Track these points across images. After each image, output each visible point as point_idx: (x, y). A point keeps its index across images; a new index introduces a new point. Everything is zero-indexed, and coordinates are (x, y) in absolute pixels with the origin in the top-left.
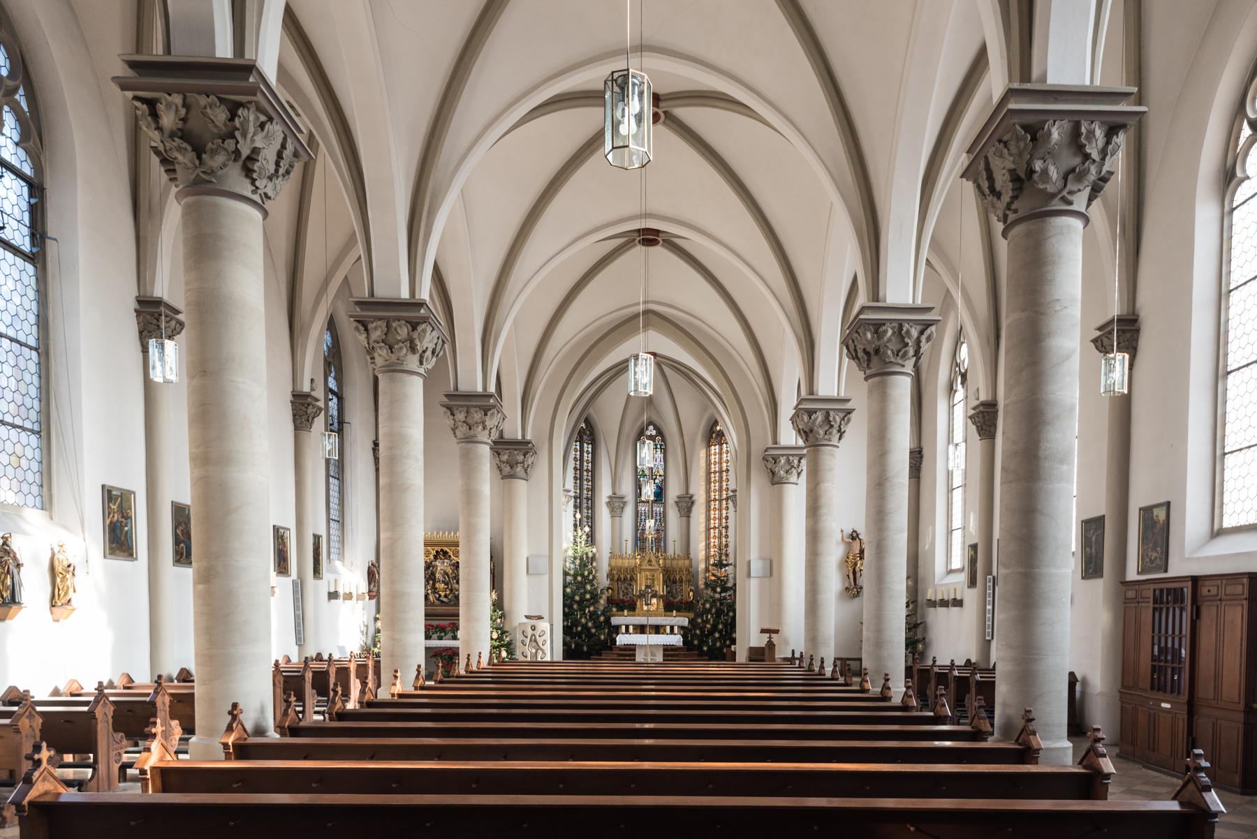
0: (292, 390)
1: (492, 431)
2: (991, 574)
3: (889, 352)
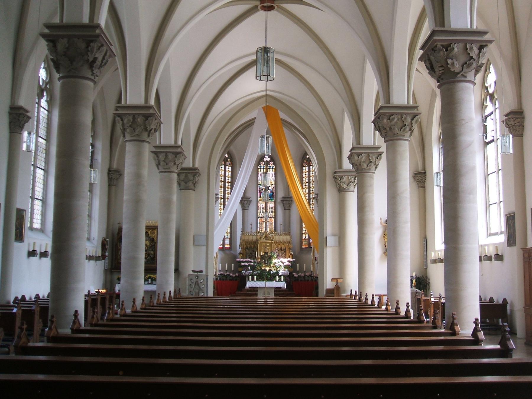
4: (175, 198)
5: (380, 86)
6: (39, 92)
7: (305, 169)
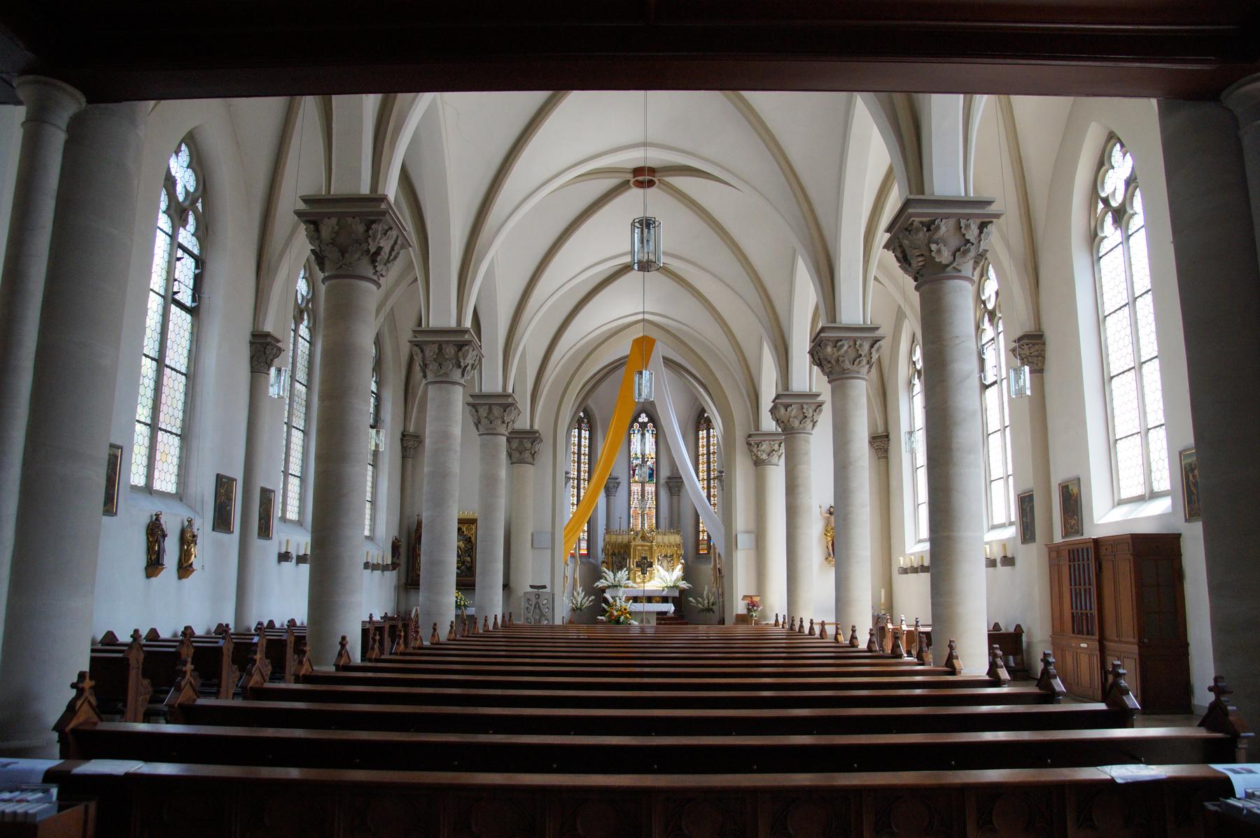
4: (503, 473)
5: (821, 295)
6: (296, 313)
7: (703, 434)
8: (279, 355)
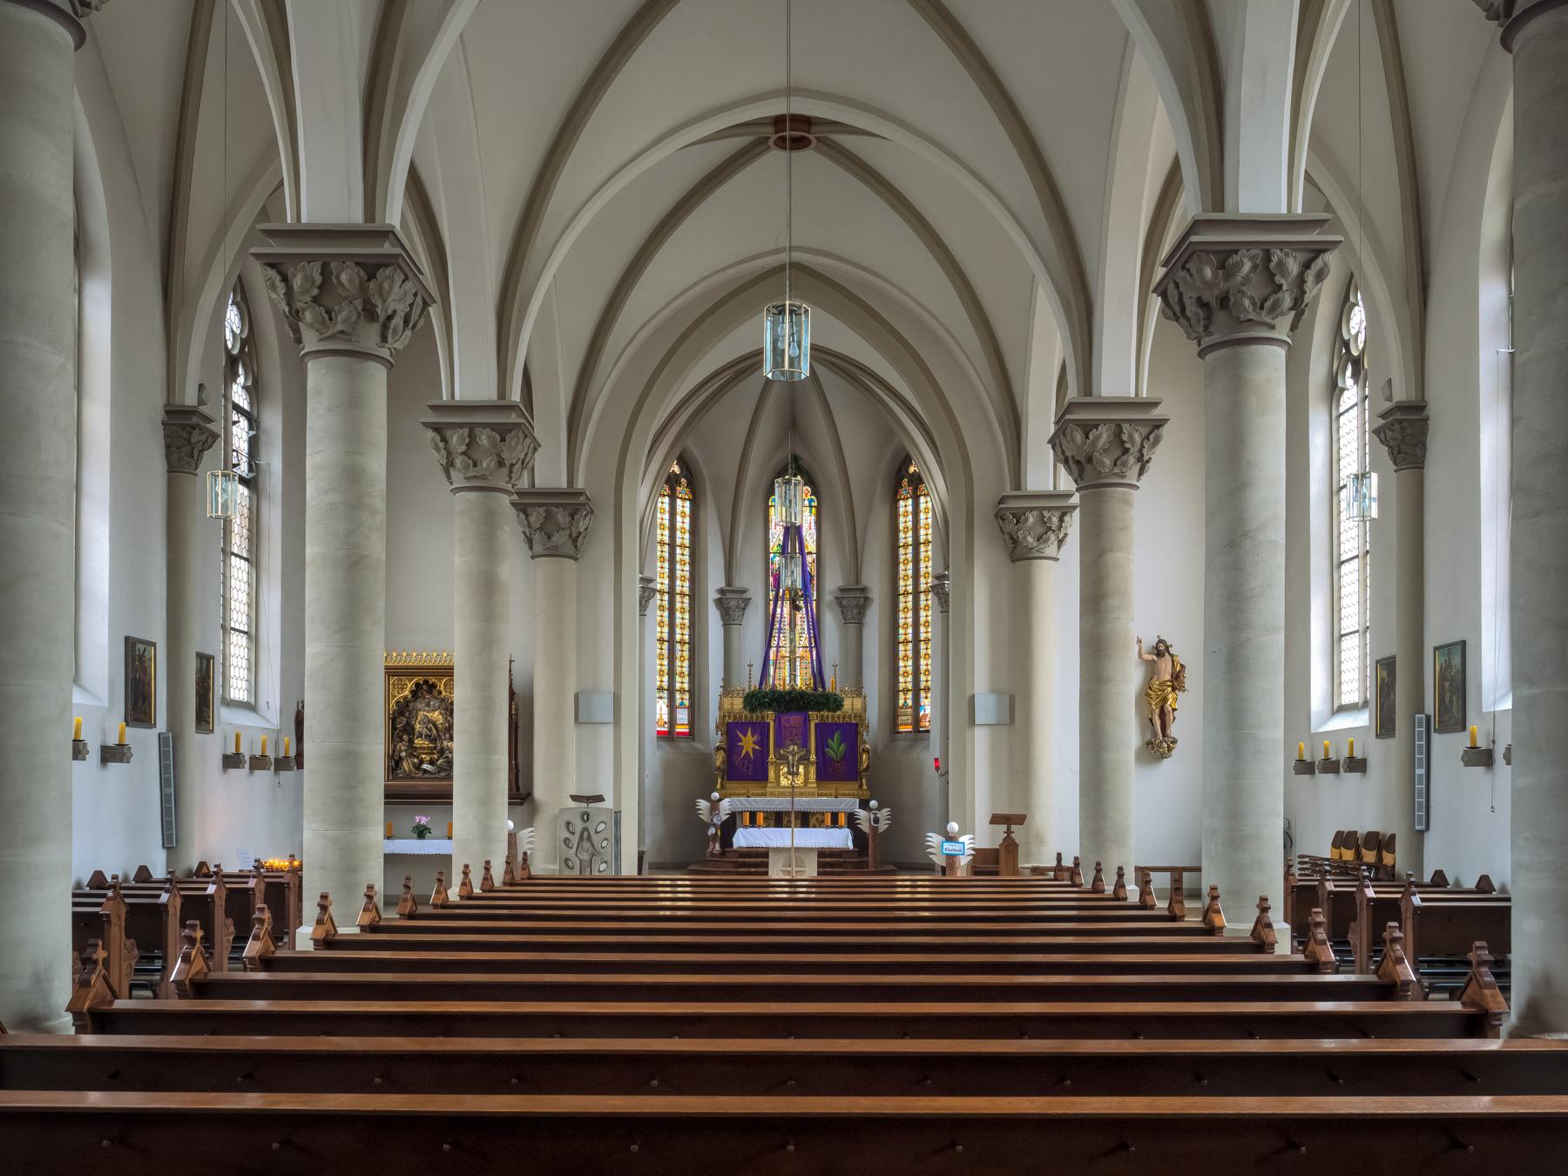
0: (164, 402)
1: (514, 470)
2: (1422, 712)
3: (1247, 302)
7: (906, 506)
8: (211, 446)
